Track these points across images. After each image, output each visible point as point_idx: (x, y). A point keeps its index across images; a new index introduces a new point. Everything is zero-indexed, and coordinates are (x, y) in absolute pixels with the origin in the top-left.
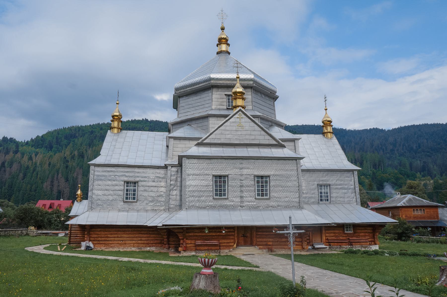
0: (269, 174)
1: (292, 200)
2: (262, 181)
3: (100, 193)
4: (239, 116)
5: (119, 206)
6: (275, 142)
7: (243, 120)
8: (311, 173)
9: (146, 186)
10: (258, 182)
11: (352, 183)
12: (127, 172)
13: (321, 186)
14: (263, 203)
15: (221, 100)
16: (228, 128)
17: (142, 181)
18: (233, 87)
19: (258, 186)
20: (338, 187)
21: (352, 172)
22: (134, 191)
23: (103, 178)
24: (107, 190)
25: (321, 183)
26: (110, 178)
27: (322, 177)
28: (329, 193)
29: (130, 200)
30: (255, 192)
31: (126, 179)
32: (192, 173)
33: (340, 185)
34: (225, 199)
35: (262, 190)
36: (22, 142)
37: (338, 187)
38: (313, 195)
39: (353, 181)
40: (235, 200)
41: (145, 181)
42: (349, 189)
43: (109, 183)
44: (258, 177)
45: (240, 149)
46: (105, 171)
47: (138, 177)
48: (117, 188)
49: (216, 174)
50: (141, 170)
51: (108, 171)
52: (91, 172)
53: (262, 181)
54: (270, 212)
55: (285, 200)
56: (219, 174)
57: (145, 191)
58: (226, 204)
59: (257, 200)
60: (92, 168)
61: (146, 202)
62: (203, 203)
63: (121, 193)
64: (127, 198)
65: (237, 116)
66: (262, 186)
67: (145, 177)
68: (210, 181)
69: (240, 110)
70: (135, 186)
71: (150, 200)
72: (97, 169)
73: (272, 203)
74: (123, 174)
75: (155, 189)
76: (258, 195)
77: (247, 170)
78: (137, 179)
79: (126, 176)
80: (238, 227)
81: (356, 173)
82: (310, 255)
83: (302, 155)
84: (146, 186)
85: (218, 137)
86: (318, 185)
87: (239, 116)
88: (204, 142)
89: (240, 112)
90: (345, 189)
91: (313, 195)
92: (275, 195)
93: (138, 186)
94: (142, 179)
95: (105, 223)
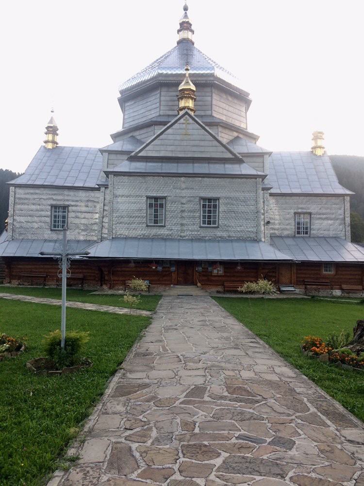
0: (219, 196)
1: (247, 230)
2: (210, 205)
3: (22, 219)
4: (184, 122)
5: (45, 235)
6: (229, 156)
7: (190, 127)
8: (288, 198)
9: (78, 212)
10: (204, 206)
11: (341, 212)
12: (55, 194)
13: (300, 214)
14: (208, 233)
15: (170, 103)
16: (171, 137)
17: (72, 206)
18: (178, 84)
19: (204, 212)
20: (322, 216)
21: (342, 198)
22: (64, 217)
23: (26, 201)
24: (30, 216)
25: (300, 211)
26: (34, 202)
27: (302, 203)
28: (309, 224)
29: (59, 229)
30: (200, 219)
31: (54, 203)
32: (121, 194)
33: (323, 214)
34: (162, 226)
35: (209, 217)
36: (15, 173)
37: (322, 216)
38: (288, 227)
39: (343, 209)
40: (173, 229)
41: (77, 206)
42: (337, 219)
43: (33, 207)
44: (204, 199)
45: (183, 165)
46: (28, 194)
47: (68, 200)
48: (43, 213)
49: (152, 195)
50: (72, 193)
51: (32, 194)
52: (11, 193)
53: (210, 205)
54: (217, 244)
55: (238, 230)
56: (155, 195)
57: (77, 217)
58: (162, 233)
59: (202, 229)
60: (12, 189)
61: (77, 231)
62: (134, 232)
63: (48, 220)
64: (55, 226)
65: (182, 121)
66: (210, 212)
67: (77, 201)
68: (143, 203)
69: (186, 113)
70: (65, 212)
71: (82, 228)
72: (18, 190)
73: (222, 233)
74: (50, 197)
75: (88, 215)
76: (204, 222)
77: (191, 191)
78: (67, 203)
79: (54, 200)
80: (170, 261)
81: (348, 198)
82: (287, 298)
83: (268, 173)
84: (78, 212)
85: (157, 148)
86: (295, 213)
87: (184, 122)
88: (140, 155)
89: (187, 116)
90: (331, 219)
91: (288, 227)
92: (226, 223)
93: (68, 211)
94: (73, 203)
95: (25, 255)
